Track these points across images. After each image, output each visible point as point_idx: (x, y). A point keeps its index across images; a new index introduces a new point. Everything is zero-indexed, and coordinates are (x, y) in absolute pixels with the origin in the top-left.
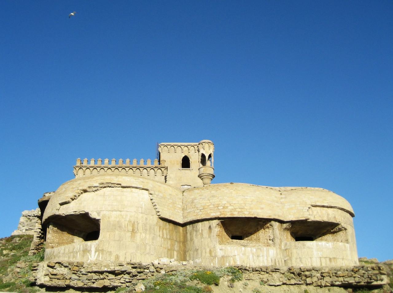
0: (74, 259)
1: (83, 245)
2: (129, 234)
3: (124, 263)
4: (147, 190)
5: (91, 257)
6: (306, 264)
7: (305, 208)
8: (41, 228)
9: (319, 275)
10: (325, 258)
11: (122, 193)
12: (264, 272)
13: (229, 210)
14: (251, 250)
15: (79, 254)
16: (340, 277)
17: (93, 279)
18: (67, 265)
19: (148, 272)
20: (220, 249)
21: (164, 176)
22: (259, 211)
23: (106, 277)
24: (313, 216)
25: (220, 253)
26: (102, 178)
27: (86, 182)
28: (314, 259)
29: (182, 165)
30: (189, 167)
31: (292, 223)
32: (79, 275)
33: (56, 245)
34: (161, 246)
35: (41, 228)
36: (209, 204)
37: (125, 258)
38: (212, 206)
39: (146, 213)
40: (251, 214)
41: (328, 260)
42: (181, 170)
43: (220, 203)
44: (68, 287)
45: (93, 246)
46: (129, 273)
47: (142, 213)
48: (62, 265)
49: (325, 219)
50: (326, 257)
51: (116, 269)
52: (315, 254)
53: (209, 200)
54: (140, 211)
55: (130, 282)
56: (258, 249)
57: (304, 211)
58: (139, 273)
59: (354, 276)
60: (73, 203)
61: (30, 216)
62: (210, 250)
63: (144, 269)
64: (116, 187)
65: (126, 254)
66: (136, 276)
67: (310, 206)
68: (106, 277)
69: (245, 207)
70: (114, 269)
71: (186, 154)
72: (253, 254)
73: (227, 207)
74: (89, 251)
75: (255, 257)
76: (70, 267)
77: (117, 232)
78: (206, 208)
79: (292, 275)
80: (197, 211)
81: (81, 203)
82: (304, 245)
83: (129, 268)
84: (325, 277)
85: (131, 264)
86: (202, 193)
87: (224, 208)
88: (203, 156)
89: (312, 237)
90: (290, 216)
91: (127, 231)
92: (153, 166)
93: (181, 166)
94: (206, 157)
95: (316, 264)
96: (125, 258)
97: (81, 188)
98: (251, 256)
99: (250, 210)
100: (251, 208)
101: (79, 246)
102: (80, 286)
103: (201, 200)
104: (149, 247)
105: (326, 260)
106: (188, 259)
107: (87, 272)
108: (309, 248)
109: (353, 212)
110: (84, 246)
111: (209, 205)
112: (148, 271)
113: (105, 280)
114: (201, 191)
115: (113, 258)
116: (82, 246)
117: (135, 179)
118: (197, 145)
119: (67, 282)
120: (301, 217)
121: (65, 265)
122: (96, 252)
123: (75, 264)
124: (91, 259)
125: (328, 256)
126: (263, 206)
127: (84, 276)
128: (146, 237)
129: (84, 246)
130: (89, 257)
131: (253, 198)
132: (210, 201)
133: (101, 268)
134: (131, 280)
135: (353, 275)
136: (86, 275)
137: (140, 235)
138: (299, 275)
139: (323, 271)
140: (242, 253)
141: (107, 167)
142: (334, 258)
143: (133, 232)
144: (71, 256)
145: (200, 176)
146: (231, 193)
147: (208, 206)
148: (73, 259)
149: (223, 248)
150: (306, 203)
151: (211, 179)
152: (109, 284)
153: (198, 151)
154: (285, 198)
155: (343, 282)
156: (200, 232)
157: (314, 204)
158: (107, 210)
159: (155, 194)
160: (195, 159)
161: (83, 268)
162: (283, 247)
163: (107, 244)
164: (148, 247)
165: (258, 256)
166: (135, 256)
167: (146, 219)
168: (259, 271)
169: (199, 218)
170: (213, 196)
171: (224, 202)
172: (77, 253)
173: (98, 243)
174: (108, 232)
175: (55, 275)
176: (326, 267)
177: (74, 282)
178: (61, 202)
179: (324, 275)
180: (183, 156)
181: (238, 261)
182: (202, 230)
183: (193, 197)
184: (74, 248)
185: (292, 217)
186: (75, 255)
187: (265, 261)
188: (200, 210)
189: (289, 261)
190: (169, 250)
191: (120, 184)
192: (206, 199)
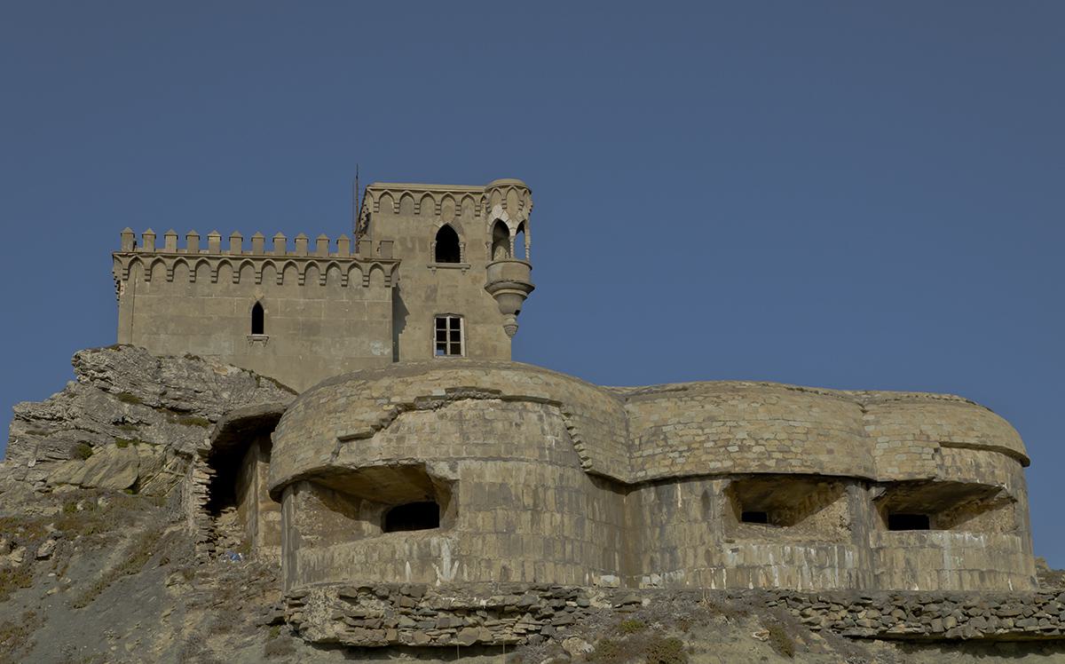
0: (397, 577)
1: (419, 545)
2: (527, 516)
3: (523, 587)
4: (558, 404)
5: (442, 573)
6: (925, 585)
7: (926, 450)
8: (210, 482)
10: (970, 571)
11: (504, 413)
12: (837, 604)
13: (755, 456)
15: (411, 567)
16: (1007, 617)
17: (452, 625)
18: (386, 593)
19: (576, 607)
21: (391, 289)
22: (824, 458)
23: (482, 621)
24: (944, 468)
25: (731, 559)
26: (453, 375)
27: (408, 384)
28: (947, 574)
29: (436, 253)
31: (891, 485)
32: (415, 617)
33: (320, 538)
34: (592, 543)
35: (210, 482)
36: (703, 438)
37: (523, 574)
38: (711, 444)
39: (560, 463)
40: (805, 466)
41: (976, 575)
42: (434, 268)
43: (731, 437)
44: (395, 648)
45: (445, 548)
46: (534, 612)
47: (551, 463)
48: (374, 593)
49: (971, 477)
50: (973, 570)
51: (507, 602)
52: (946, 561)
53: (703, 429)
54: (548, 459)
55: (538, 631)
56: (821, 549)
57: (924, 456)
58: (556, 609)
59: (1038, 615)
60: (377, 439)
61: (38, 418)
62: (708, 552)
63: (567, 600)
64: (488, 398)
65: (523, 566)
66: (550, 616)
67: (937, 445)
68: (482, 621)
69: (793, 449)
70: (504, 601)
71: (448, 219)
72: (810, 561)
73: (750, 447)
74: (437, 560)
75: (814, 570)
76: (392, 598)
77: (500, 512)
78: (694, 449)
79: (900, 613)
80: (671, 455)
81: (401, 439)
83: (529, 599)
84: (973, 617)
85: (539, 590)
86: (679, 409)
87: (742, 448)
88: (500, 226)
89: (928, 515)
90: (890, 469)
91: (521, 508)
92: (357, 256)
93: (434, 257)
94: (510, 231)
95: (951, 585)
96: (523, 574)
97: (396, 399)
98: (805, 568)
99: (805, 457)
100: (805, 452)
101: (407, 547)
102: (423, 642)
103: (681, 426)
104: (570, 546)
105: (971, 575)
107: (437, 610)
108: (933, 546)
109: (1021, 450)
110: (422, 546)
111: (704, 442)
112: (574, 604)
113: (479, 628)
114: (676, 403)
115: (494, 575)
116: (415, 547)
117: (531, 378)
118: (481, 193)
119: (392, 636)
120: (918, 471)
121: (380, 592)
122: (453, 562)
123: (404, 591)
125: (977, 568)
127: (429, 618)
128: (562, 522)
129: (422, 546)
130: (438, 572)
131: (808, 425)
132: (703, 431)
133: (471, 600)
134: (539, 627)
135: (1035, 613)
136: (432, 616)
137: (551, 517)
138: (917, 612)
139: (969, 604)
141: (219, 259)
142: (990, 571)
143: (536, 510)
144: (386, 570)
145: (491, 288)
146: (756, 411)
147: (702, 442)
148: (395, 578)
149: (740, 547)
150: (928, 437)
151: (520, 298)
152: (490, 638)
154: (877, 423)
155: (1014, 629)
156: (680, 505)
157: (946, 439)
158: (472, 458)
159: (576, 414)
160: (474, 234)
161: (426, 600)
162: (871, 542)
163: (480, 542)
164: (569, 548)
165: (821, 567)
166: (543, 568)
167: (562, 476)
168: (827, 603)
169: (678, 471)
170: (712, 419)
171: (741, 435)
172: (403, 564)
173: (457, 539)
174: (480, 511)
175: (362, 618)
176: (976, 593)
177: (407, 633)
178: (342, 434)
179: (971, 612)
180: (441, 225)
181: (776, 580)
183: (655, 417)
184: (395, 552)
185: (896, 470)
186: (401, 568)
188: (681, 452)
189: (885, 578)
190: (605, 549)
191: (498, 392)
192: (695, 425)
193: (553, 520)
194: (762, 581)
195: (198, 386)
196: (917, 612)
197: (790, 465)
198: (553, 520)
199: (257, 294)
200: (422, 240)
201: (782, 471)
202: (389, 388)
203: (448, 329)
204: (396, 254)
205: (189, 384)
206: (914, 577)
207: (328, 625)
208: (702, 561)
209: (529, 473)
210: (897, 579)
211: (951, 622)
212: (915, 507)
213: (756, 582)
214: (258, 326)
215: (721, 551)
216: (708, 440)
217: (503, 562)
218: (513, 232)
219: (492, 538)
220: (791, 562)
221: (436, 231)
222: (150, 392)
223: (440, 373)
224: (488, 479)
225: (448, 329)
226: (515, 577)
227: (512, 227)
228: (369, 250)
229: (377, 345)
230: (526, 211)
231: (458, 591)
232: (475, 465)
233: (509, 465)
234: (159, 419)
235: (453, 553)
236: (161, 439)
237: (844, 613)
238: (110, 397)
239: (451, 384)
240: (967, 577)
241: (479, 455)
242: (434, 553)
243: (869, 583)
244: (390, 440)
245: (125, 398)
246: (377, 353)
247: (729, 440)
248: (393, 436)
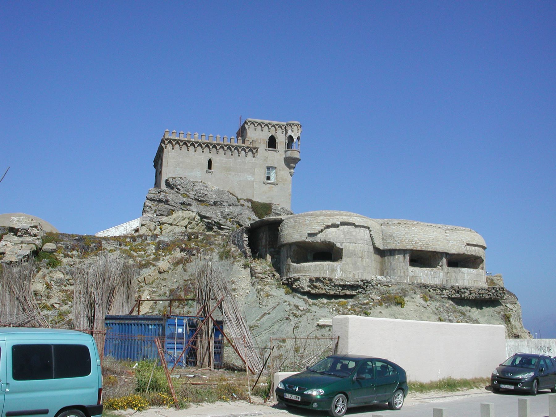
3: (359, 280)
9: (468, 292)
25: (411, 274)
28: (465, 281)
74: (336, 271)
88: (291, 138)
95: (466, 284)
97: (326, 224)
106: (385, 275)
108: (462, 273)
126: (439, 243)
140: (424, 275)
153: (287, 132)
160: (281, 139)
193: (366, 261)
194: (419, 280)
195: (206, 193)
196: (458, 292)
198: (366, 261)
199: (210, 156)
200: (264, 140)
202: (322, 220)
204: (255, 145)
205: (203, 192)
206: (457, 281)
208: (402, 274)
210: (452, 281)
211: (466, 294)
212: (457, 261)
214: (210, 167)
217: (354, 272)
218: (295, 140)
219: (351, 265)
220: (427, 276)
222: (192, 194)
223: (338, 217)
224: (351, 248)
226: (356, 277)
227: (295, 139)
228: (247, 144)
230: (299, 133)
232: (348, 244)
234: (194, 203)
236: (195, 210)
237: (439, 291)
238: (180, 195)
239: (342, 221)
240: (470, 281)
242: (335, 269)
243: (445, 282)
246: (249, 179)
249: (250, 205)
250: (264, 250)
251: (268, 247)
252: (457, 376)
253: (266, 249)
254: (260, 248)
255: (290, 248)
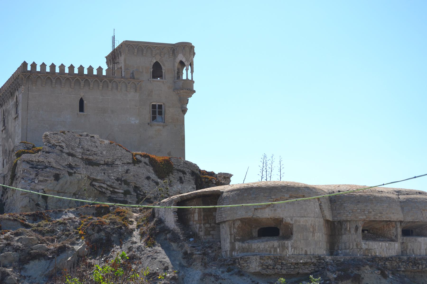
2: (311, 234)
14: (385, 245)
20: (153, 120)
28: (422, 251)
30: (183, 53)
36: (357, 208)
38: (359, 211)
45: (289, 244)
62: (357, 244)
72: (386, 248)
74: (287, 248)
82: (416, 240)
93: (151, 77)
108: (419, 242)
122: (292, 249)
124: (289, 254)
143: (313, 233)
147: (356, 210)
182: (350, 228)
187: (393, 253)
197: (383, 218)
201: (380, 220)
203: (157, 110)
207: (257, 267)
209: (312, 221)
213: (371, 254)
214: (81, 109)
215: (361, 244)
216: (358, 209)
219: (302, 241)
221: (152, 64)
224: (302, 223)
225: (157, 110)
229: (133, 119)
231: (293, 257)
233: (307, 219)
235: (292, 246)
238: (64, 154)
241: (299, 216)
244: (271, 210)
245: (69, 154)
246: (133, 122)
247: (365, 209)
248: (272, 209)
249: (147, 160)
250: (198, 225)
251: (203, 222)
252: (416, 176)
253: (200, 224)
254: (191, 223)
255: (234, 224)
